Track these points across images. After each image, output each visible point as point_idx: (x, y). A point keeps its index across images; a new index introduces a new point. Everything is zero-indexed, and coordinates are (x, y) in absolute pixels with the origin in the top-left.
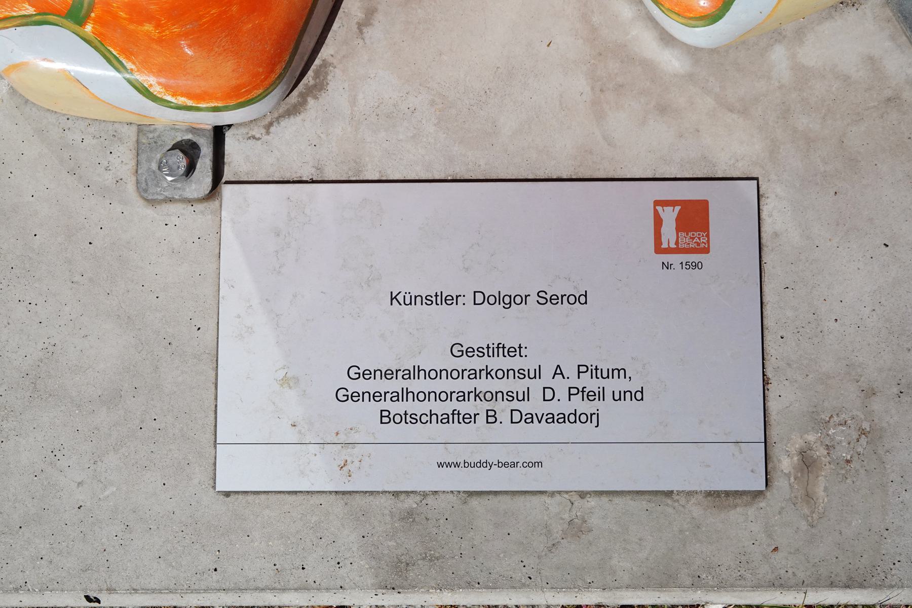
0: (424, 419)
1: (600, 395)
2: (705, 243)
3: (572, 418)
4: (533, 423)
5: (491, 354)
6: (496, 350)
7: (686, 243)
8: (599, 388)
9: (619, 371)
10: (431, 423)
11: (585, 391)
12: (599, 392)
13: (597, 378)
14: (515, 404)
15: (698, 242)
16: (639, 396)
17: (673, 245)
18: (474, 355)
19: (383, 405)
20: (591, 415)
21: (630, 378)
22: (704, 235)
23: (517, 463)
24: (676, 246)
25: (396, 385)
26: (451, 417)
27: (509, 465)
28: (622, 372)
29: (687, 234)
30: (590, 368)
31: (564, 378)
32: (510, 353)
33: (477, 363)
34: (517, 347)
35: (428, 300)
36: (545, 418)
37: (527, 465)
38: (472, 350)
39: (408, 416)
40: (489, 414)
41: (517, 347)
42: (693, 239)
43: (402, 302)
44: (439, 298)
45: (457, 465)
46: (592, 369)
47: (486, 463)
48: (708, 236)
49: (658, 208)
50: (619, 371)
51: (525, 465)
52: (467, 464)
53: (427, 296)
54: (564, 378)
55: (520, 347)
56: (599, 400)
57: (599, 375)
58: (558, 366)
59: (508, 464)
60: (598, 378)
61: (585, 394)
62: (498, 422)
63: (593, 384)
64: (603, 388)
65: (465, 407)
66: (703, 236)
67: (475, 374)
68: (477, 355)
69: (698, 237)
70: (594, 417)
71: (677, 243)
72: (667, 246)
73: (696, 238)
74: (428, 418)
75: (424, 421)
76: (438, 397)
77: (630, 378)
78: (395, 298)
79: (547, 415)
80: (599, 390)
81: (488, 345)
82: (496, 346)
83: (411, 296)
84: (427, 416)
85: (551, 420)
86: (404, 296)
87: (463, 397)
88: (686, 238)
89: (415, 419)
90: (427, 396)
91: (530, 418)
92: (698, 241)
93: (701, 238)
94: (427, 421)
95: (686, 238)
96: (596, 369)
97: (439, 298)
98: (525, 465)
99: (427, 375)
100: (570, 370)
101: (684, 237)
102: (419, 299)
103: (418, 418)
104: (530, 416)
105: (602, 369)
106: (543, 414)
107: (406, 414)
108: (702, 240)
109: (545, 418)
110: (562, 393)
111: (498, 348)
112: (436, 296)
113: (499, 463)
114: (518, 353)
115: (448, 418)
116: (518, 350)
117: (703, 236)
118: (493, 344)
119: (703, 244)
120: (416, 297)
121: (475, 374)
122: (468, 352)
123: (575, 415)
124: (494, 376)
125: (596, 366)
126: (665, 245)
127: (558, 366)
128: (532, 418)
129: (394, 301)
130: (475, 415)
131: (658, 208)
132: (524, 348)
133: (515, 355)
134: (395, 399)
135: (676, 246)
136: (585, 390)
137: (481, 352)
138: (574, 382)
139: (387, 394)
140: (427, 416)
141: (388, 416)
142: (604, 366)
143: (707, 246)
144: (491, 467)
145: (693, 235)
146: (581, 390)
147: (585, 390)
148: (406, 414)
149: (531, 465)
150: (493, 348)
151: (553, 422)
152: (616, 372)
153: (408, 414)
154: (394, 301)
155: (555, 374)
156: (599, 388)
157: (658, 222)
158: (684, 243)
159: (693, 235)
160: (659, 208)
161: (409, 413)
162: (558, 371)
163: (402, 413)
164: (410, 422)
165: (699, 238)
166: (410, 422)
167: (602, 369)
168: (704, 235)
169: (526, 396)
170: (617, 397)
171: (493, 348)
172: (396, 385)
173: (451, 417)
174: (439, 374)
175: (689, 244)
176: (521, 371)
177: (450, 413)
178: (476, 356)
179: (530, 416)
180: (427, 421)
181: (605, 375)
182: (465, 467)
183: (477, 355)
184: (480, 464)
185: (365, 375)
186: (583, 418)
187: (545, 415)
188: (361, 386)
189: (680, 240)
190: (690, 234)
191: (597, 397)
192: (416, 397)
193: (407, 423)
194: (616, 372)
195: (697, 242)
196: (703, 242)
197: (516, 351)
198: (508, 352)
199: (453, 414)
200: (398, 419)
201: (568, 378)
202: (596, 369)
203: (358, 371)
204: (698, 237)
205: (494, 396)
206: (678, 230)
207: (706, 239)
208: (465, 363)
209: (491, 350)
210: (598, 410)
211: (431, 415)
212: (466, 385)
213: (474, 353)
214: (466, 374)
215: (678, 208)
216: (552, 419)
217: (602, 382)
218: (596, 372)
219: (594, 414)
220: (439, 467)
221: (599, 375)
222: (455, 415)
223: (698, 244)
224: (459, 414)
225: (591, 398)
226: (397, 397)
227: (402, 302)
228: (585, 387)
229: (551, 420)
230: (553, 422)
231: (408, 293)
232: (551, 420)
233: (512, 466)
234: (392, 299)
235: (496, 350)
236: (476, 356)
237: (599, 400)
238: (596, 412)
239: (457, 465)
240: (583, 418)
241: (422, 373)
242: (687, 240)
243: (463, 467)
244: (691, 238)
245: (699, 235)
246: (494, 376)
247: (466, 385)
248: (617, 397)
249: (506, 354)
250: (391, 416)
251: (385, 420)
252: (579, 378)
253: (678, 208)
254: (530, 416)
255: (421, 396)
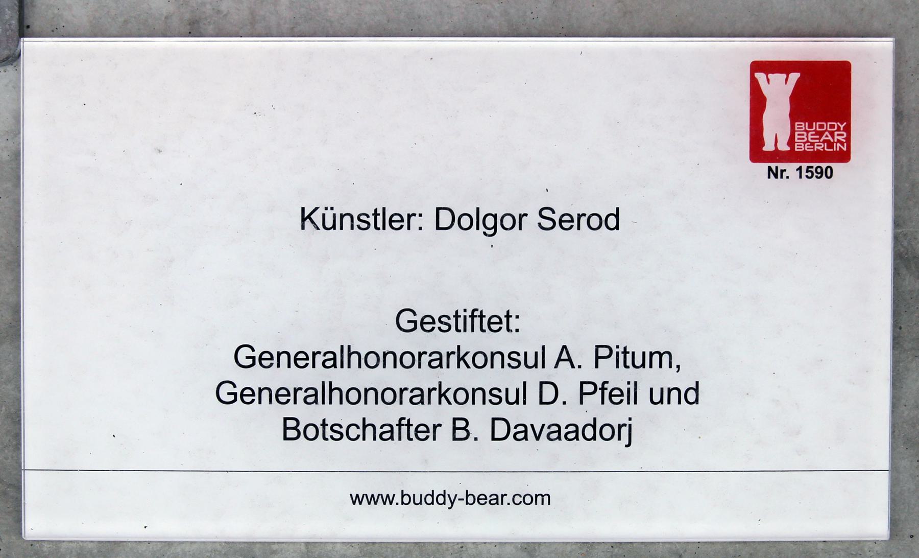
0: (354, 432)
1: (631, 395)
2: (842, 143)
3: (589, 432)
4: (527, 440)
5: (461, 327)
6: (469, 320)
7: (808, 141)
8: (629, 383)
9: (661, 355)
10: (364, 439)
11: (606, 389)
12: (629, 390)
13: (626, 367)
14: (503, 410)
15: (829, 140)
16: (691, 396)
17: (783, 147)
18: (433, 328)
19: (290, 410)
20: (620, 427)
21: (678, 367)
22: (842, 127)
23: (502, 496)
24: (788, 149)
25: (313, 377)
26: (396, 429)
27: (488, 501)
28: (666, 358)
29: (810, 126)
30: (615, 350)
31: (573, 366)
32: (492, 326)
33: (445, 342)
34: (502, 315)
35: (362, 222)
36: (546, 431)
37: (521, 499)
38: (498, 321)
39: (328, 429)
40: (457, 426)
41: (502, 315)
42: (821, 134)
43: (320, 225)
44: (380, 218)
45: (388, 500)
46: (618, 353)
47: (444, 496)
48: (848, 129)
49: (757, 75)
50: (661, 355)
51: (518, 499)
52: (407, 499)
53: (360, 215)
54: (573, 366)
55: (508, 316)
56: (629, 403)
57: (629, 363)
58: (564, 347)
59: (486, 498)
60: (628, 367)
61: (607, 393)
62: (472, 437)
63: (619, 378)
64: (636, 383)
65: (419, 415)
66: (839, 129)
67: (439, 360)
68: (439, 328)
69: (829, 132)
70: (625, 431)
71: (791, 142)
72: (772, 148)
73: (827, 133)
74: (360, 432)
75: (353, 436)
76: (379, 397)
77: (678, 367)
78: (309, 217)
79: (549, 427)
80: (629, 386)
81: (457, 312)
82: (469, 313)
83: (334, 215)
84: (358, 427)
85: (556, 435)
86: (324, 215)
87: (420, 397)
88: (808, 132)
89: (339, 433)
90: (363, 395)
91: (523, 433)
92: (830, 138)
93: (836, 133)
94: (358, 436)
95: (808, 132)
96: (625, 352)
97: (380, 218)
98: (518, 499)
99: (363, 361)
100: (583, 355)
101: (805, 131)
102: (347, 219)
103: (343, 431)
104: (522, 428)
105: (633, 353)
106: (543, 426)
107: (324, 424)
108: (836, 137)
109: (546, 431)
110: (569, 391)
111: (473, 316)
112: (376, 214)
113: (467, 496)
114: (504, 325)
115: (392, 431)
116: (504, 320)
117: (839, 129)
118: (465, 310)
119: (839, 145)
120: (342, 216)
121: (439, 360)
122: (425, 324)
123: (594, 427)
124: (470, 364)
125: (625, 348)
126: (769, 147)
127: (564, 347)
128: (526, 431)
129: (308, 222)
130: (435, 427)
131: (757, 75)
132: (514, 317)
133: (500, 328)
134: (310, 400)
135: (788, 149)
136: (606, 386)
137: (444, 324)
138: (589, 373)
139: (299, 392)
140: (358, 427)
141: (295, 428)
142: (638, 347)
143: (845, 149)
144: (452, 503)
145: (821, 126)
146: (599, 386)
147: (606, 386)
148: (324, 424)
149: (528, 500)
150: (465, 317)
151: (559, 438)
152: (656, 357)
153: (327, 425)
154: (308, 222)
155: (559, 360)
156: (629, 383)
157: (758, 102)
158: (804, 143)
159: (821, 126)
160: (761, 77)
161: (329, 422)
162: (564, 356)
163: (319, 423)
164: (332, 437)
165: (832, 134)
166: (332, 437)
167: (633, 353)
168: (842, 127)
169: (521, 397)
170: (657, 398)
171: (465, 317)
172: (313, 377)
173: (396, 429)
174: (382, 359)
175: (812, 144)
176: (514, 356)
177: (394, 422)
178: (436, 330)
179: (522, 428)
180: (358, 436)
181: (638, 362)
182: (403, 503)
183: (439, 328)
184: (433, 499)
185: (264, 360)
186: (607, 432)
187: (546, 427)
188: (257, 378)
189: (797, 137)
190: (816, 125)
191: (625, 398)
192: (344, 397)
193: (327, 439)
194: (656, 357)
195: (828, 141)
196: (839, 141)
197: (501, 322)
198: (489, 323)
199: (400, 425)
200: (311, 432)
201: (580, 367)
202: (625, 352)
203: (251, 354)
204: (829, 132)
205: (471, 396)
206: (795, 116)
207: (845, 136)
208: (419, 341)
209: (461, 320)
210: (630, 419)
211: (365, 426)
212: (424, 378)
213: (433, 326)
214: (425, 359)
215: (795, 77)
216: (557, 433)
217: (632, 374)
218: (624, 357)
219: (625, 425)
220: (354, 503)
221: (629, 363)
222: (402, 427)
223: (830, 145)
224: (409, 425)
225: (616, 399)
226: (314, 397)
227: (320, 225)
228: (607, 382)
229: (556, 435)
230: (559, 438)
231: (329, 208)
232: (555, 435)
233: (494, 502)
234: (304, 220)
235: (469, 320)
236: (436, 330)
237: (629, 403)
238: (628, 423)
239: (388, 500)
240: (607, 432)
241: (354, 357)
242: (810, 137)
243: (400, 503)
244: (817, 133)
245: (832, 126)
246: (470, 364)
247: (424, 378)
248: (657, 398)
249: (485, 327)
250: (301, 428)
251: (291, 434)
252: (597, 366)
253: (795, 77)
254: (522, 428)
255: (353, 396)
